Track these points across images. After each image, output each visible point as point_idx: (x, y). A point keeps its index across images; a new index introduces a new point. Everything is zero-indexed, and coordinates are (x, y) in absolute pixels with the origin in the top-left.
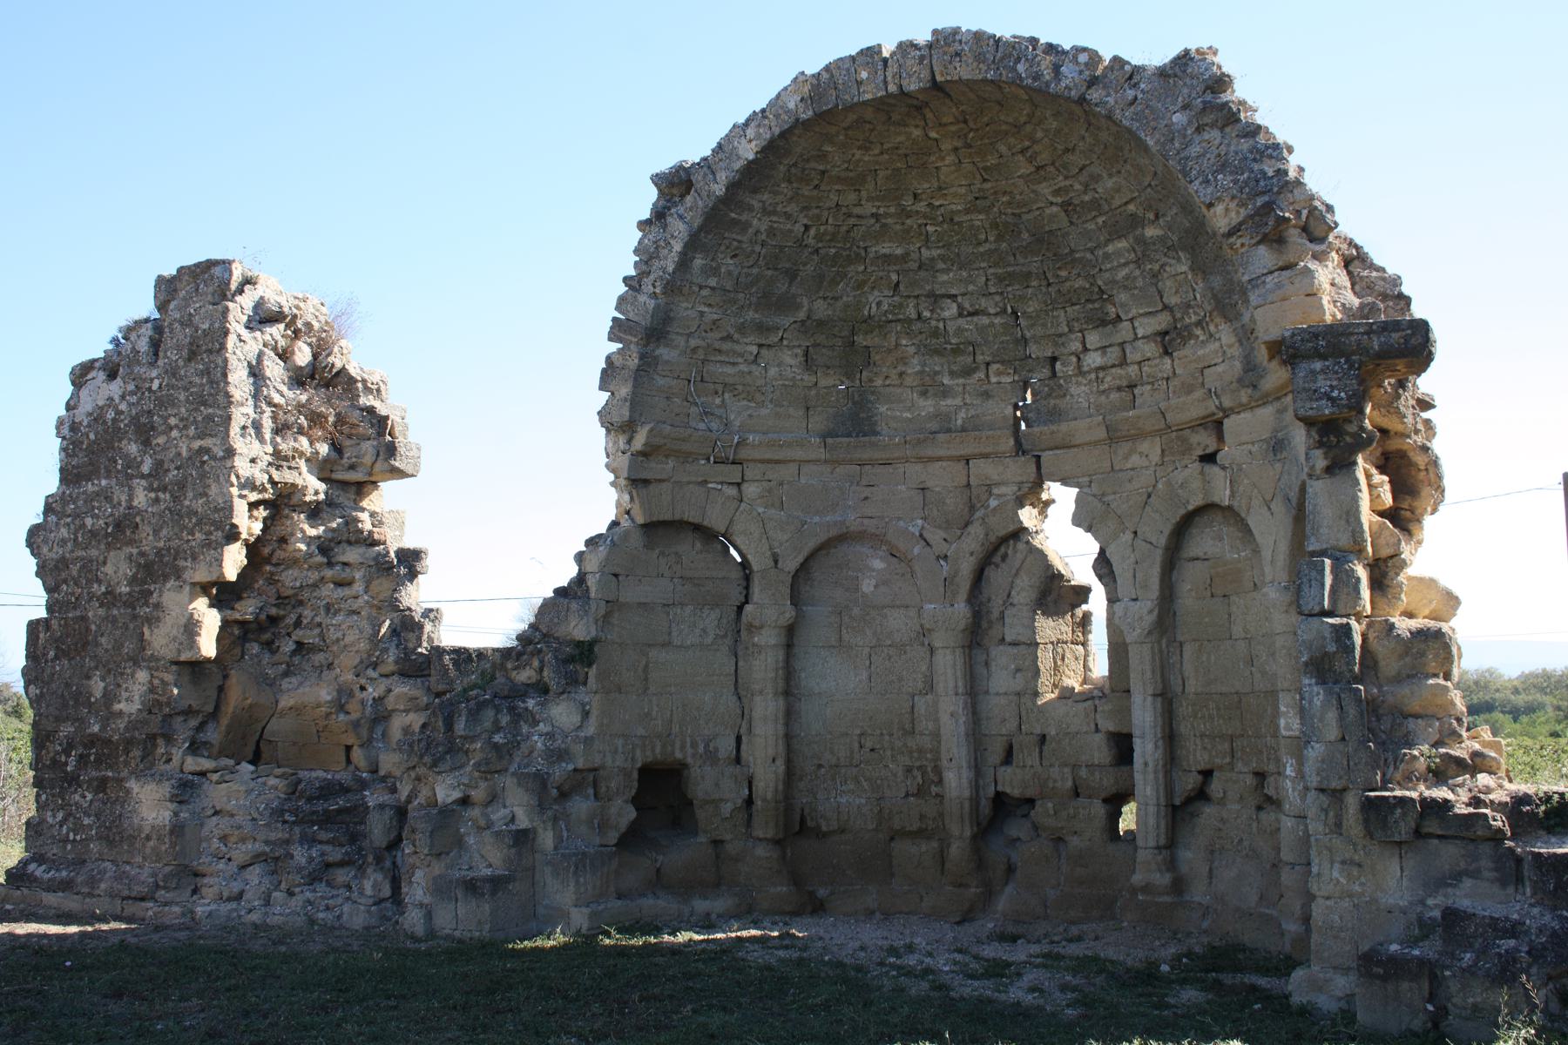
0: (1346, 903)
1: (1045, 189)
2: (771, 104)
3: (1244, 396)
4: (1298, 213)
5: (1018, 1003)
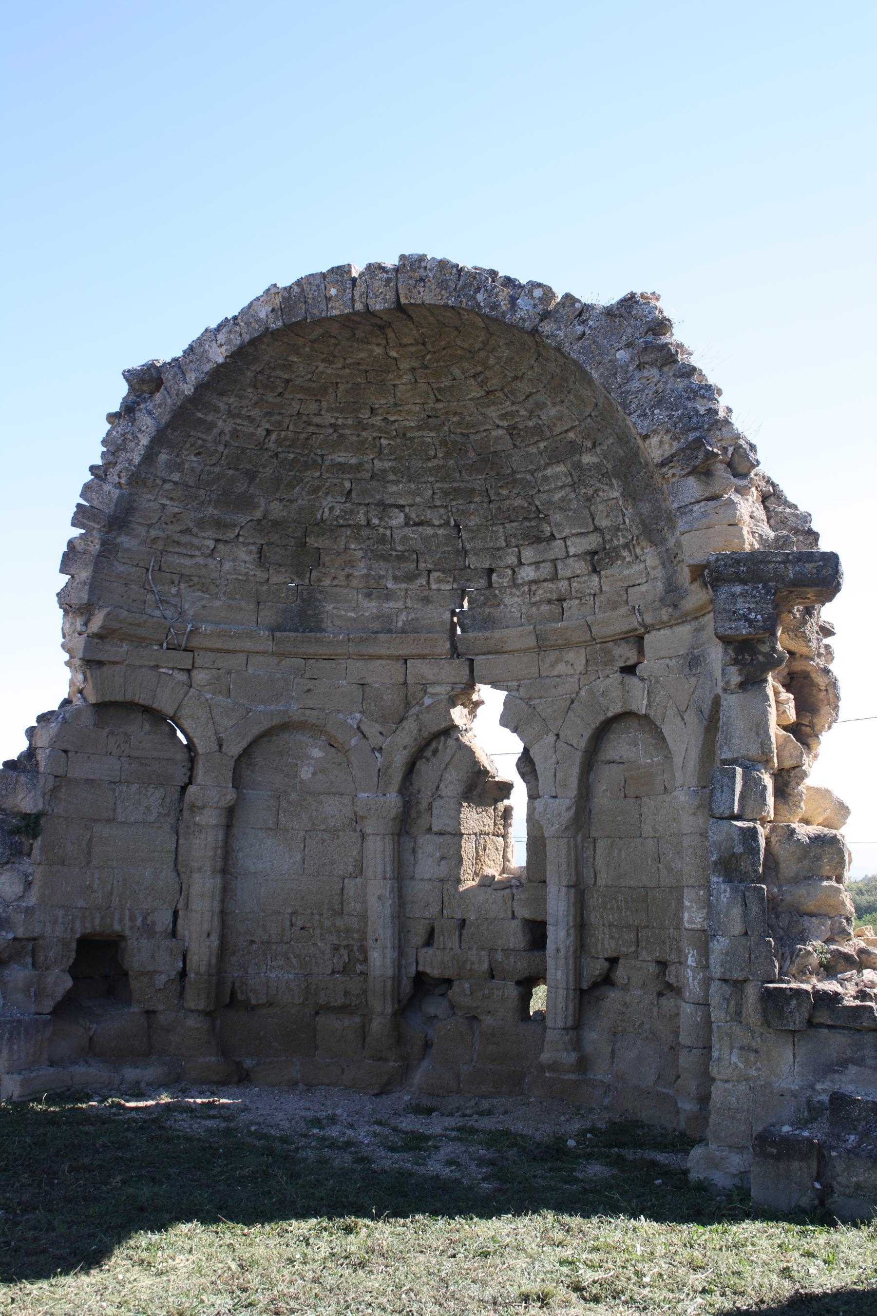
0: (743, 1087)
1: (493, 413)
2: (243, 312)
3: (665, 614)
4: (725, 449)
5: (437, 1176)
